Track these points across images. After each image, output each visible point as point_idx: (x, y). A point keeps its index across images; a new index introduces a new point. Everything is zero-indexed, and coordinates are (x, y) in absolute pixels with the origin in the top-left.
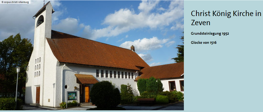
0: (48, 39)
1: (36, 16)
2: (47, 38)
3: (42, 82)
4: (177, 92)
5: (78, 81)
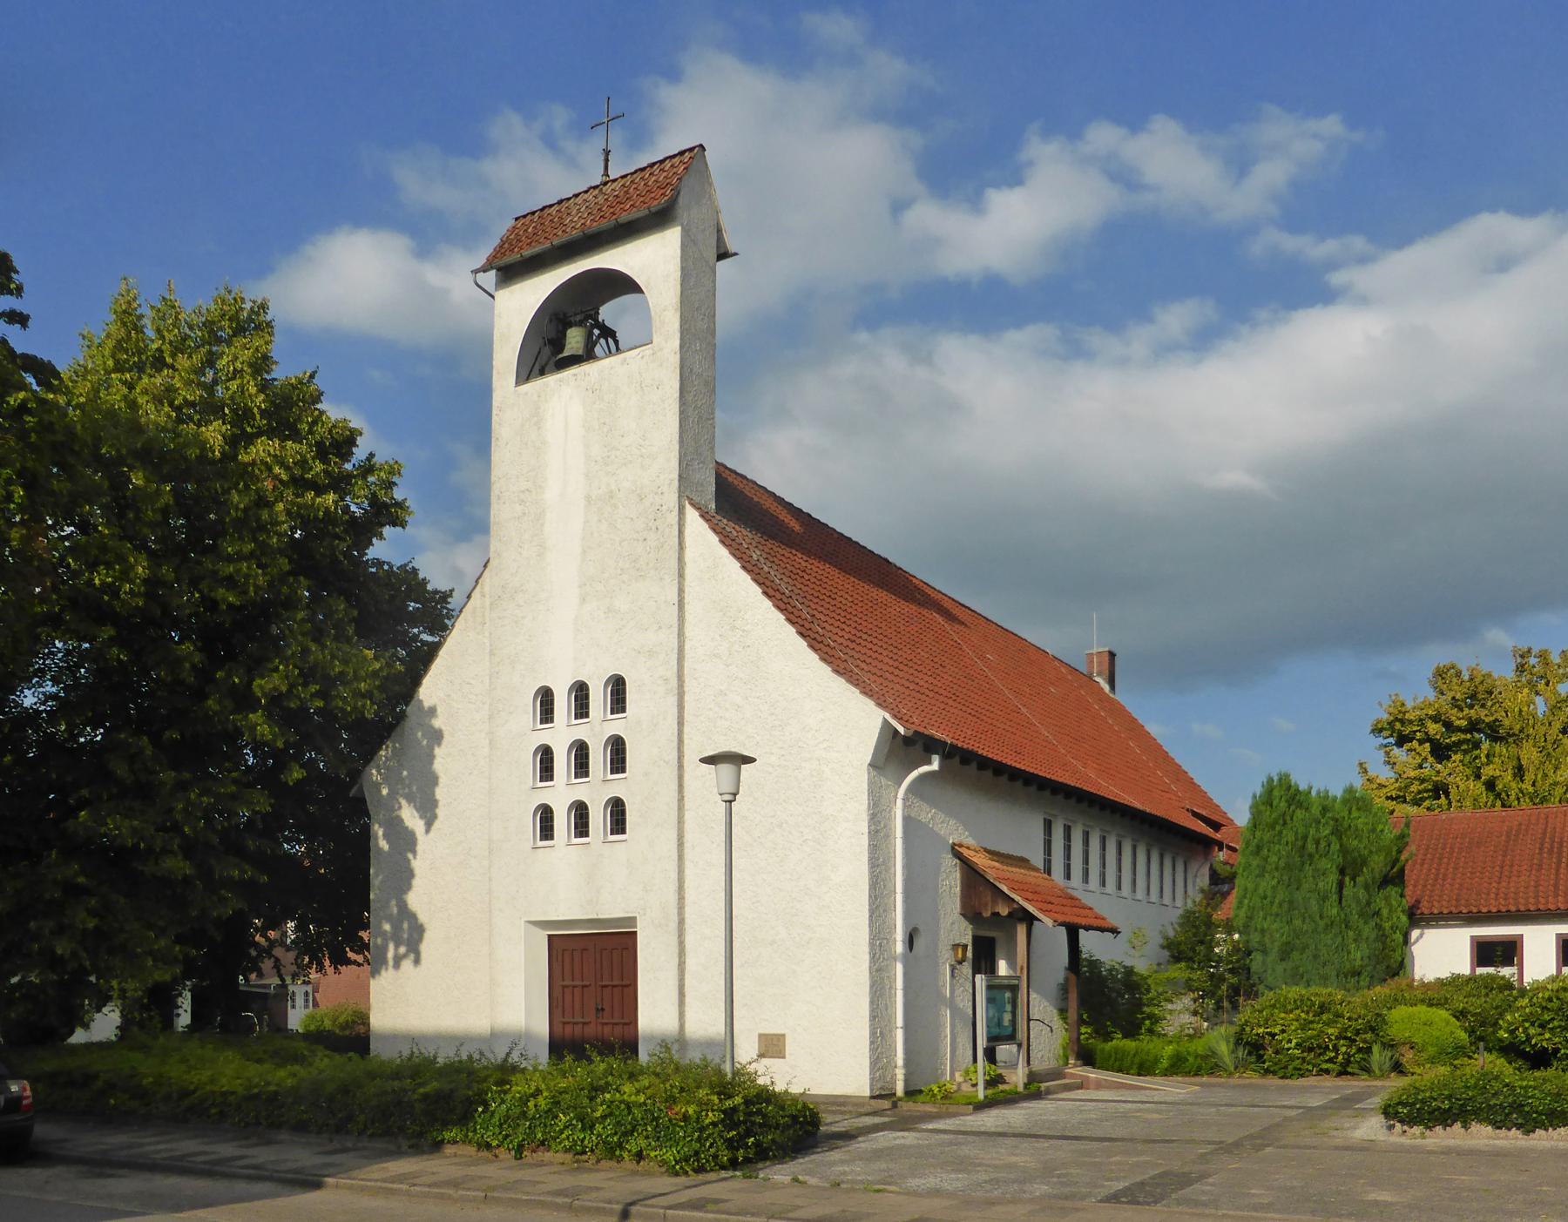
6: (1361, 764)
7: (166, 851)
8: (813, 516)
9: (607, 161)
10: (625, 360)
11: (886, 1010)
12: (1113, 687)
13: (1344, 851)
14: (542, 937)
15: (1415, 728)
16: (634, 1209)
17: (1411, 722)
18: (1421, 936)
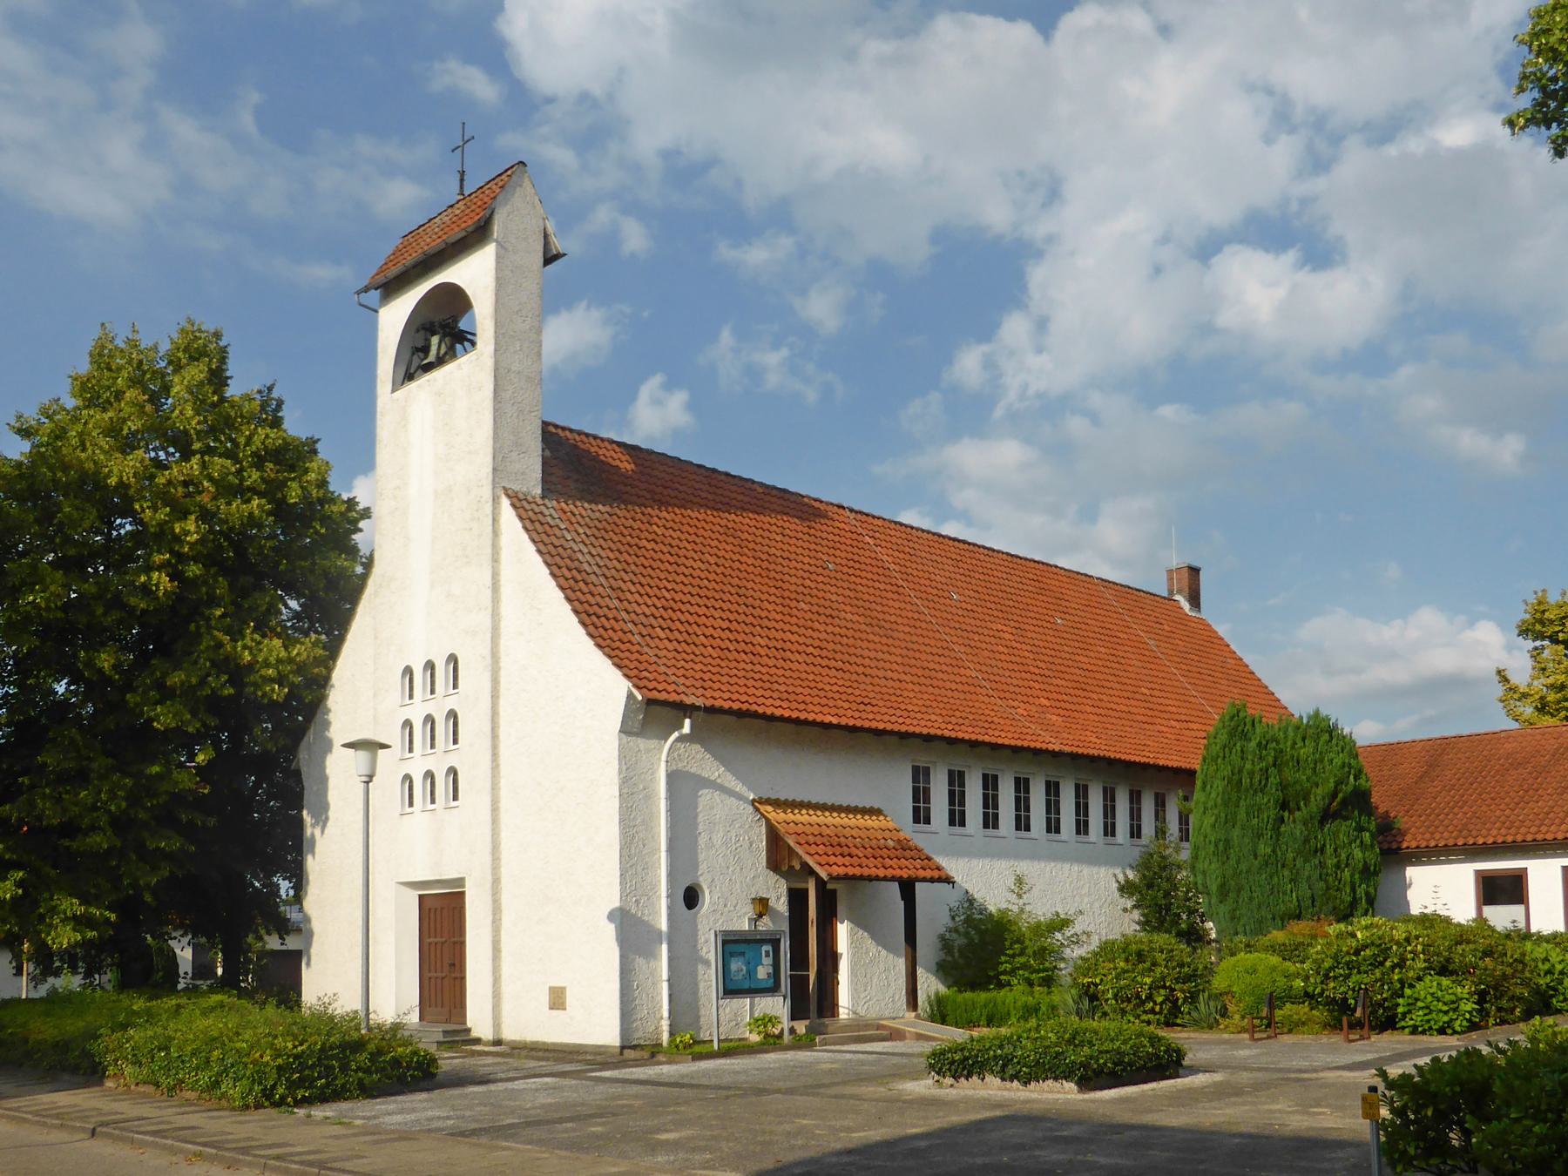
0: (519, 503)
1: (391, 286)
2: (508, 496)
3: (487, 859)
4: (1499, 933)
5: (778, 854)
6: (1499, 672)
7: (93, 828)
8: (733, 473)
9: (462, 180)
10: (459, 365)
12: (1195, 600)
13: (1283, 786)
14: (413, 897)
15: (1557, 629)
16: (98, 1129)
17: (1551, 622)
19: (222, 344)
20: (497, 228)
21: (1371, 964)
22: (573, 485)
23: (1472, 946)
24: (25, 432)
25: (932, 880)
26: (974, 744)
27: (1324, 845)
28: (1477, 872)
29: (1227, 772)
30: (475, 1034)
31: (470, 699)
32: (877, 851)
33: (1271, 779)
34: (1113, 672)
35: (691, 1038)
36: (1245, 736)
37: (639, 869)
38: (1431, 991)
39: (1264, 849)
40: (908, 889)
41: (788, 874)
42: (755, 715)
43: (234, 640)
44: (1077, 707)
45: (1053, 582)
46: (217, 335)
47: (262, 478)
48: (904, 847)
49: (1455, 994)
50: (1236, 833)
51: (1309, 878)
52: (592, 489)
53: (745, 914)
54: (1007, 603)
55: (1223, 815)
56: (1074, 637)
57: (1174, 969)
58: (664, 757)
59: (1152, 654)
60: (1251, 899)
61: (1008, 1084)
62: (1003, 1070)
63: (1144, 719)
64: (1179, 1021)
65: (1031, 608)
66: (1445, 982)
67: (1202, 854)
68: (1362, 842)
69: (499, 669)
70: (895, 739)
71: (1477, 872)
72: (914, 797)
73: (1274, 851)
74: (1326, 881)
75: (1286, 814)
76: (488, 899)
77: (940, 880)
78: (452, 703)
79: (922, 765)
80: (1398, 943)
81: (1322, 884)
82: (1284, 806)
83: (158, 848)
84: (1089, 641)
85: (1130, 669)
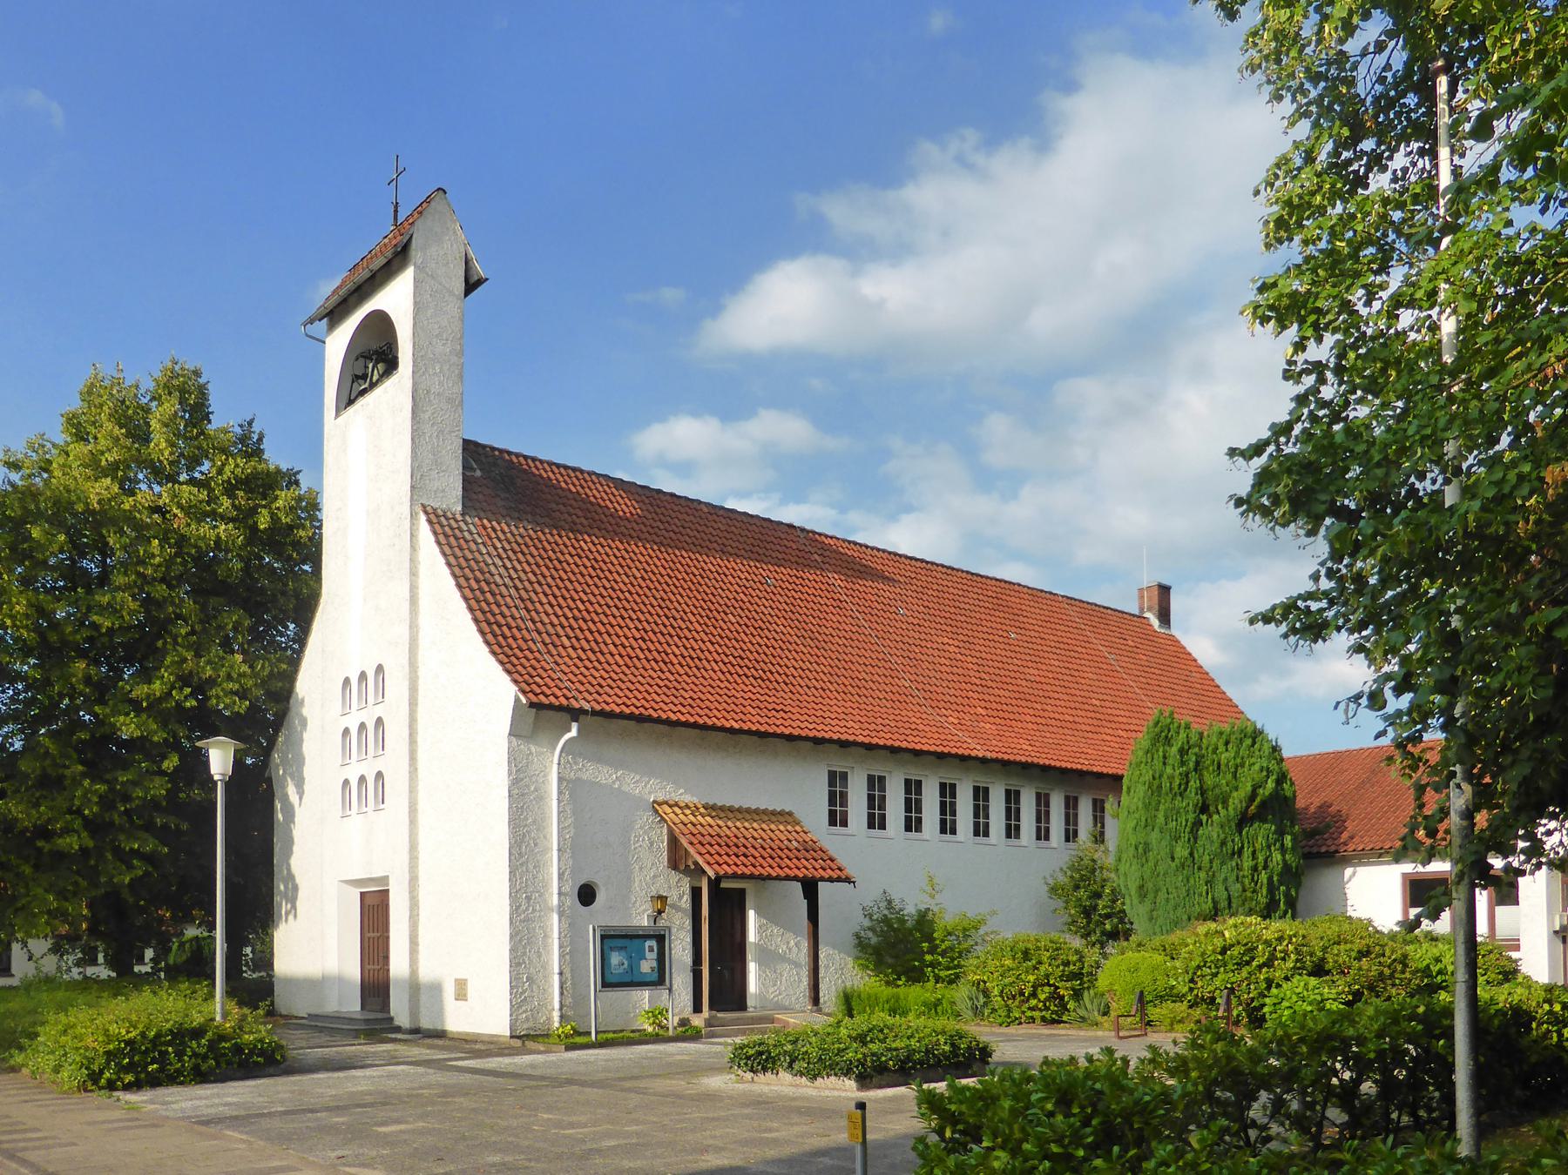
0: (436, 519)
1: (335, 314)
2: (426, 512)
11: (539, 957)
12: (1165, 616)
13: (1202, 791)
14: (354, 896)
18: (1354, 874)
19: (202, 381)
20: (416, 253)
21: (1237, 964)
22: (501, 503)
23: (1348, 946)
24: (14, 466)
25: (831, 880)
26: (894, 750)
27: (1243, 847)
28: (1405, 875)
29: (1148, 777)
30: (397, 1022)
31: (394, 709)
32: (777, 852)
33: (1192, 783)
34: (1062, 683)
35: (572, 1028)
36: (1168, 741)
37: (531, 867)
38: (1298, 991)
39: (1181, 851)
40: (810, 889)
41: (687, 871)
42: (649, 719)
43: (198, 655)
44: (1017, 717)
45: (1013, 599)
46: (197, 373)
47: (233, 505)
48: (811, 849)
49: (1322, 995)
50: (1154, 836)
51: (1226, 879)
52: (521, 507)
53: (645, 911)
54: (959, 618)
55: (1143, 819)
56: (1027, 651)
57: (1058, 966)
58: (556, 760)
59: (1109, 667)
60: (1167, 900)
61: (798, 1080)
62: (790, 1066)
63: (1088, 728)
64: (1065, 1018)
65: (984, 623)
66: (1313, 981)
67: (1124, 856)
68: (1283, 845)
69: (417, 677)
70: (809, 744)
71: (1405, 875)
72: (830, 801)
73: (1191, 854)
74: (1242, 883)
75: (1204, 818)
76: (406, 895)
77: (839, 880)
78: (379, 711)
79: (877, 774)
80: (1268, 943)
81: (1238, 886)
82: (1204, 809)
83: (132, 849)
84: (1041, 654)
85: (1083, 681)
